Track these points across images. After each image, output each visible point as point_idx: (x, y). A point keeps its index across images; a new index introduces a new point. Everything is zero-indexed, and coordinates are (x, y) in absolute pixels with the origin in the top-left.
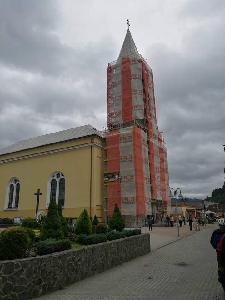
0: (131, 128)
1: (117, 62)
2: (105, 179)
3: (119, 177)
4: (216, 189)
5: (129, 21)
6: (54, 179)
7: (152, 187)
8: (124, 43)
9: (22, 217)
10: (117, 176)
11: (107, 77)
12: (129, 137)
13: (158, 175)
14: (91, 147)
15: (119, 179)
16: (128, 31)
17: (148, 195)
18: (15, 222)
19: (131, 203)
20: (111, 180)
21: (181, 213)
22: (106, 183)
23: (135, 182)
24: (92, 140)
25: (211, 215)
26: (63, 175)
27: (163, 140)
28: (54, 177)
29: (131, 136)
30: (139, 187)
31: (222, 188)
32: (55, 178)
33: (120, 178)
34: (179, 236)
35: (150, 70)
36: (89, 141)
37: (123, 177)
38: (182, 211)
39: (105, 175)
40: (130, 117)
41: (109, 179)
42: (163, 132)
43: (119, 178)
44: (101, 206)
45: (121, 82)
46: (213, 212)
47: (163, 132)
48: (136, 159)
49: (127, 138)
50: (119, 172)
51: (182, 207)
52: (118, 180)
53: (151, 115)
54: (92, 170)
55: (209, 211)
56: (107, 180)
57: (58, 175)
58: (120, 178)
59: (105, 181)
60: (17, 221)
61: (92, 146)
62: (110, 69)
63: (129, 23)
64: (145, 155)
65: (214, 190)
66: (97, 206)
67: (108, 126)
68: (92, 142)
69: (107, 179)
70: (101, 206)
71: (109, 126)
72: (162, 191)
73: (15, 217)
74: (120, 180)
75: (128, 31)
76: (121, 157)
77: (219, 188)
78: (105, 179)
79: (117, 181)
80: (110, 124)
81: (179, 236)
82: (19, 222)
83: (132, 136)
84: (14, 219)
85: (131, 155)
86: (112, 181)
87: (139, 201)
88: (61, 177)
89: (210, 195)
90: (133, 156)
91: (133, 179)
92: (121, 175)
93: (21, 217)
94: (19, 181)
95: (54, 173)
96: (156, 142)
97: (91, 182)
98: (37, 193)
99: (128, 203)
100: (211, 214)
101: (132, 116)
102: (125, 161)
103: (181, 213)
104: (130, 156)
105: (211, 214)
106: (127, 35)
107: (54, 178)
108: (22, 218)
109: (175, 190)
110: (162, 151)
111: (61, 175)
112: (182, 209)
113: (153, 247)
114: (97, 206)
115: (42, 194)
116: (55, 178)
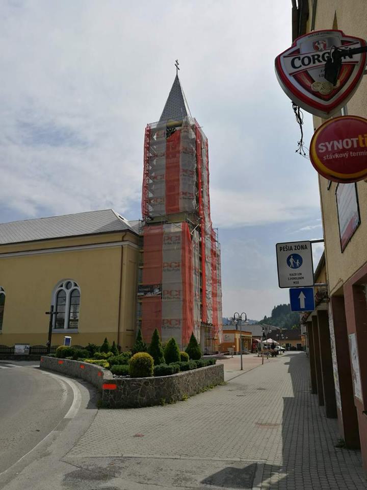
0: (180, 225)
1: (158, 125)
2: (139, 294)
3: (160, 291)
4: (279, 305)
5: (178, 62)
6: (62, 290)
7: (201, 306)
8: (170, 95)
9: (28, 344)
10: (157, 291)
11: (145, 144)
12: (177, 237)
13: (209, 289)
14: (122, 247)
15: (159, 294)
16: (177, 78)
17: (196, 315)
18: (16, 351)
19: (175, 327)
20: (149, 295)
21: (234, 341)
22: (141, 299)
23: (182, 299)
24: (123, 237)
25: (273, 346)
26: (76, 285)
27: (217, 240)
28: (62, 286)
29: (179, 236)
30: (186, 308)
31: (287, 304)
32: (64, 288)
33: (161, 293)
34: (242, 369)
35: (204, 139)
36: (118, 237)
37: (166, 292)
38: (235, 339)
39: (139, 288)
40: (176, 207)
41: (146, 293)
42: (217, 229)
43: (160, 292)
44: (132, 330)
45: (165, 156)
46: (275, 342)
47: (217, 229)
48: (183, 265)
49: (174, 239)
50: (161, 285)
51: (234, 333)
52: (159, 296)
53: (203, 205)
54: (120, 281)
55: (270, 339)
56: (142, 296)
57: (68, 285)
58: (161, 293)
59: (139, 296)
60: (19, 350)
61: (123, 246)
62: (149, 133)
63: (178, 66)
64: (195, 262)
65: (276, 306)
66: (127, 330)
67: (143, 216)
68: (123, 241)
69: (142, 294)
70: (132, 330)
71: (145, 216)
72: (213, 311)
73: (16, 344)
74: (160, 296)
75: (177, 78)
76: (164, 263)
77: (283, 305)
78: (139, 294)
79: (157, 297)
80: (146, 214)
81: (242, 369)
82: (23, 351)
83: (181, 237)
84: (14, 346)
85: (177, 262)
86: (150, 297)
87: (185, 323)
88: (73, 287)
89: (269, 315)
90: (181, 264)
91: (179, 295)
92: (163, 289)
93: (26, 344)
94: (3, 290)
95: (63, 280)
96: (208, 243)
97: (120, 297)
98: (49, 311)
99: (171, 328)
100: (273, 343)
101: (180, 206)
102: (168, 270)
103: (234, 341)
104: (176, 263)
105: (273, 343)
106: (174, 83)
107: (61, 288)
108: (27, 346)
109: (240, 315)
110: (215, 254)
111: (73, 285)
112: (235, 336)
113: (225, 379)
114: (127, 330)
115: (47, 313)
116: (64, 288)
